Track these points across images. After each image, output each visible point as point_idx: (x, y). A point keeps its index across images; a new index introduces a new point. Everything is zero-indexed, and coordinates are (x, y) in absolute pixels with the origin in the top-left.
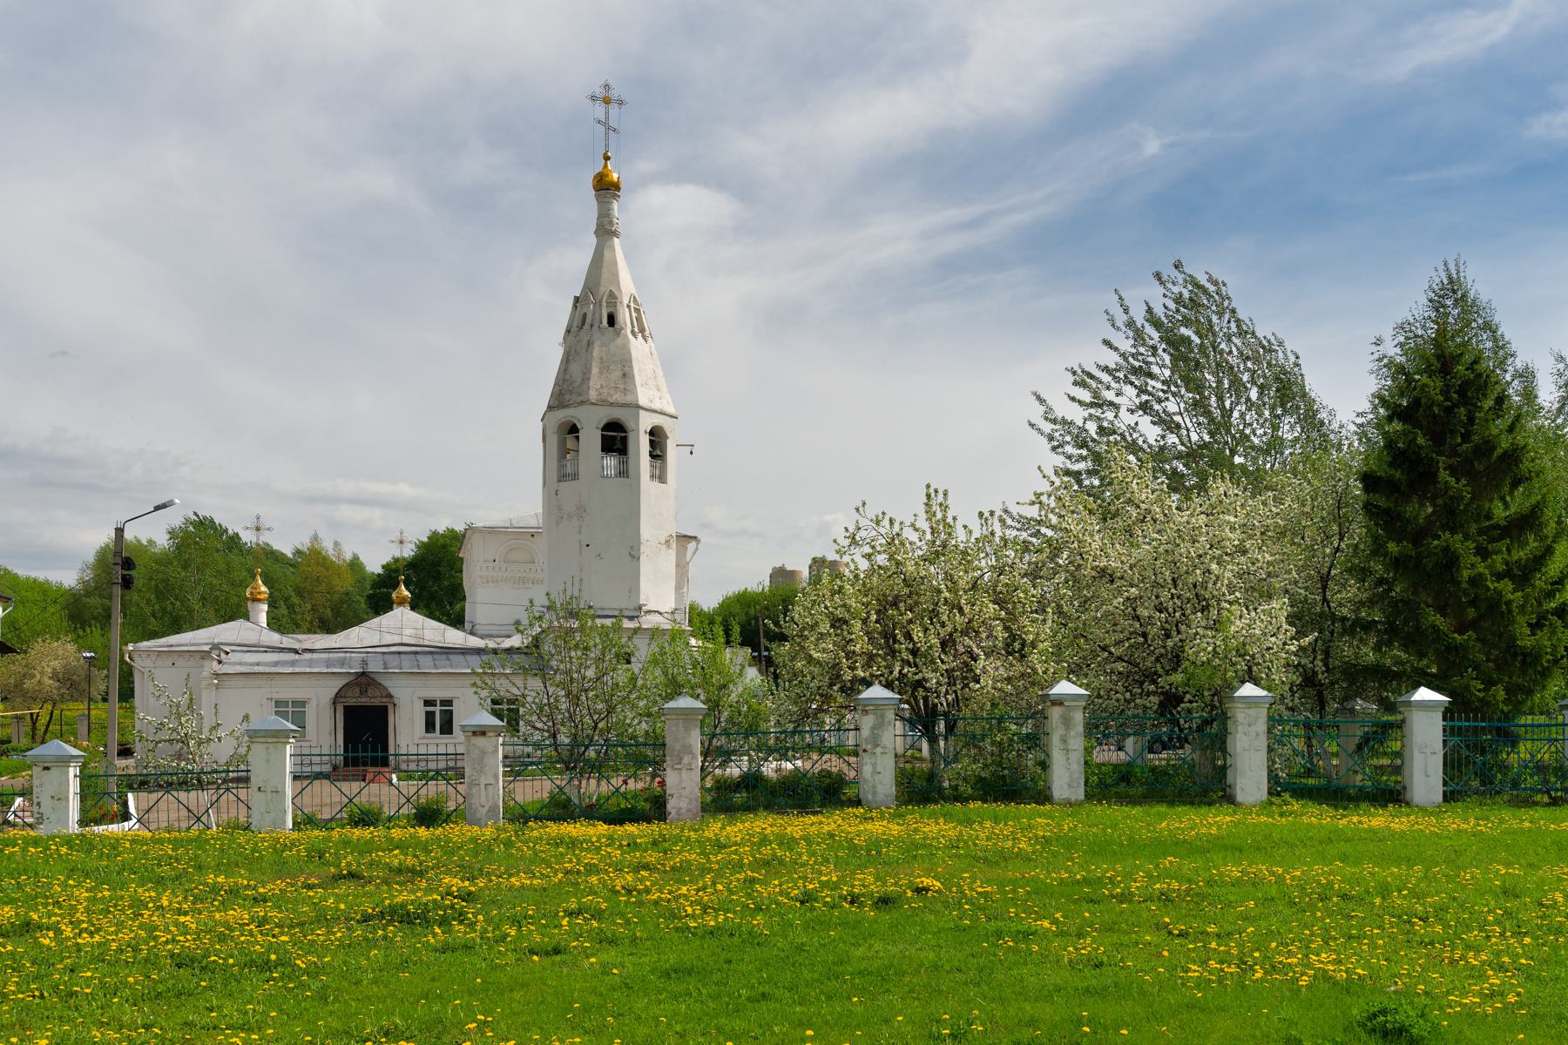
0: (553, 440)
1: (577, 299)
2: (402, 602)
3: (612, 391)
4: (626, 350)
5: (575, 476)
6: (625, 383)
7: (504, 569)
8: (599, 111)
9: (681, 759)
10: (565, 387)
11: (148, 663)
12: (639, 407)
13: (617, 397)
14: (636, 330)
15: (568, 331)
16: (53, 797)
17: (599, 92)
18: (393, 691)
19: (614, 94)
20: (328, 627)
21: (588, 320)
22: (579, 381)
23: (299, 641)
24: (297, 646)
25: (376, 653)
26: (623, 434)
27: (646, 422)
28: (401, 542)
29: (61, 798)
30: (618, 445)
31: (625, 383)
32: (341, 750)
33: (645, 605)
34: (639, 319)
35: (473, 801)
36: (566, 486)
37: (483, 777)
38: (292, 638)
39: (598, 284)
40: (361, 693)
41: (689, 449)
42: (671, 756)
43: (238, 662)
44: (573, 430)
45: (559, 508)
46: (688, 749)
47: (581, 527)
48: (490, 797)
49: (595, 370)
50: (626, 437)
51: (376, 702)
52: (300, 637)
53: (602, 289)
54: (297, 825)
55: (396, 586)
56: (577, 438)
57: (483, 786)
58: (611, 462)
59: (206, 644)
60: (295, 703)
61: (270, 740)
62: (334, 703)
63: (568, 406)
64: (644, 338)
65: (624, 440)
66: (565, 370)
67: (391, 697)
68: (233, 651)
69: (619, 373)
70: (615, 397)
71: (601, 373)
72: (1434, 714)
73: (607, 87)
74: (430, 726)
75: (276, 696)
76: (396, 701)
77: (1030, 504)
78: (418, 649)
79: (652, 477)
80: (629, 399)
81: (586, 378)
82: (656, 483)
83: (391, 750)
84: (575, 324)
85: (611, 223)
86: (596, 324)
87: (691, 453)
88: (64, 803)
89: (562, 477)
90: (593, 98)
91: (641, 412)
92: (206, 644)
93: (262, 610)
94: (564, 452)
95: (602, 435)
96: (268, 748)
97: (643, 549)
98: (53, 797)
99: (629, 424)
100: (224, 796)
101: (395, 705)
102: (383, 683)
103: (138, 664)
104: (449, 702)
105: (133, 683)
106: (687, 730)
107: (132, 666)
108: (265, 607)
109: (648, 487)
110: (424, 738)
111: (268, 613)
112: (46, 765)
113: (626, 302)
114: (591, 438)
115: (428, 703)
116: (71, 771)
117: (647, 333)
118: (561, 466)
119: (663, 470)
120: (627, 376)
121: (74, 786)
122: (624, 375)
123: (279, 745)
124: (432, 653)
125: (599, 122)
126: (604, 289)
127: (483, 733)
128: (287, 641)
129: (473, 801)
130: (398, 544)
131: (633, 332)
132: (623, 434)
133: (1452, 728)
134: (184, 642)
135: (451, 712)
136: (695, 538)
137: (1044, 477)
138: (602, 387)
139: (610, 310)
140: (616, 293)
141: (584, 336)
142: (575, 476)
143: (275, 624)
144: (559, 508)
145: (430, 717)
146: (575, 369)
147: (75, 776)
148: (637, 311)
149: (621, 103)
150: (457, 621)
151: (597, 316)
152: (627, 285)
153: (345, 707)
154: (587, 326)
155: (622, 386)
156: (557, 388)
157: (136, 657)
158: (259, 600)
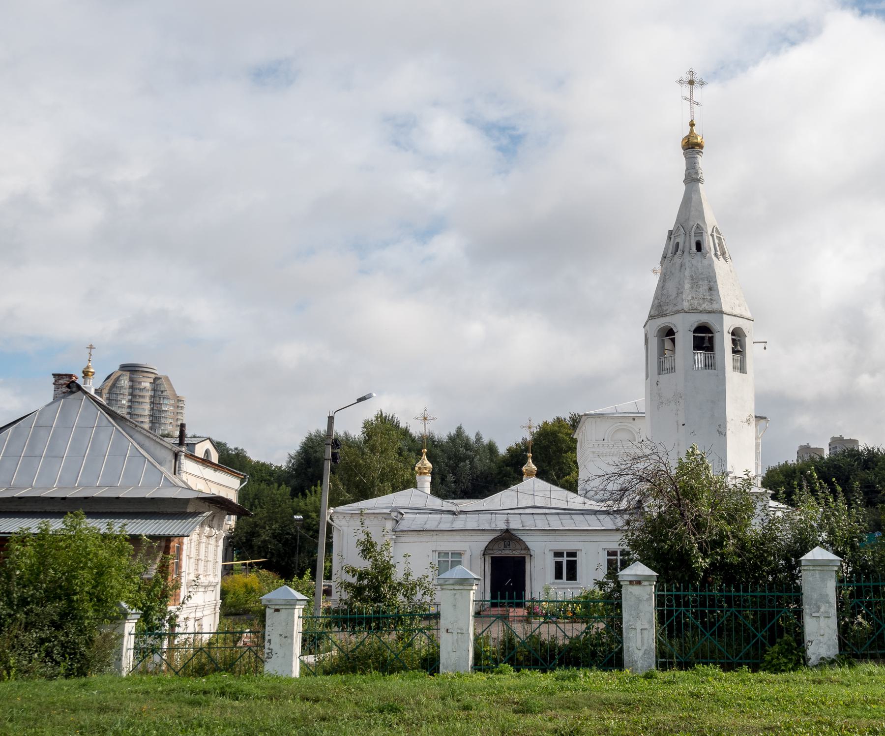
0: (654, 342)
1: (671, 233)
2: (530, 474)
3: (701, 301)
4: (711, 266)
5: (672, 369)
6: (711, 295)
7: (611, 446)
8: (686, 90)
9: (819, 607)
10: (663, 300)
11: (343, 522)
12: (722, 313)
13: (706, 306)
14: (719, 253)
15: (664, 257)
16: (281, 635)
17: (686, 77)
18: (529, 544)
19: (696, 78)
20: (467, 494)
21: (680, 247)
22: (674, 294)
23: (456, 505)
24: (454, 509)
25: (514, 514)
27: (729, 323)
28: (425, 419)
29: (287, 637)
30: (706, 344)
31: (711, 295)
32: (488, 596)
33: (731, 472)
34: (720, 244)
35: (631, 644)
36: (665, 377)
37: (639, 622)
38: (447, 502)
39: (687, 220)
40: (505, 547)
41: (763, 345)
42: (809, 604)
43: (410, 521)
44: (669, 333)
45: (660, 396)
46: (824, 598)
47: (678, 410)
48: (645, 642)
49: (687, 286)
50: (712, 337)
51: (516, 553)
52: (456, 501)
53: (691, 223)
54: (481, 662)
55: (524, 462)
56: (673, 340)
57: (639, 631)
58: (700, 357)
59: (387, 508)
60: (454, 554)
61: (457, 587)
62: (484, 554)
63: (666, 315)
64: (725, 259)
65: (711, 340)
66: (663, 287)
67: (529, 549)
68: (406, 513)
69: (706, 287)
70: (703, 306)
71: (692, 287)
73: (691, 72)
74: (558, 575)
75: (439, 549)
76: (532, 553)
78: (547, 511)
79: (735, 368)
80: (715, 307)
81: (679, 293)
82: (737, 374)
83: (528, 596)
84: (670, 251)
85: (697, 173)
86: (687, 250)
87: (765, 348)
88: (289, 641)
89: (661, 371)
90: (681, 82)
91: (724, 315)
92: (387, 508)
93: (426, 481)
94: (662, 353)
95: (694, 336)
96: (455, 594)
97: (728, 426)
98: (281, 635)
99: (715, 326)
101: (531, 556)
102: (521, 538)
103: (336, 524)
104: (572, 554)
105: (332, 537)
106: (823, 580)
107: (332, 525)
108: (429, 478)
109: (732, 377)
110: (553, 584)
111: (432, 483)
112: (277, 607)
113: (710, 232)
114: (685, 339)
115: (558, 554)
116: (296, 611)
117: (727, 256)
118: (660, 363)
119: (743, 362)
120: (712, 288)
121: (298, 626)
122: (710, 289)
123: (464, 592)
124: (558, 514)
125: (686, 99)
126: (693, 223)
127: (639, 583)
128: (448, 505)
129: (631, 644)
130: (422, 421)
131: (716, 255)
134: (370, 506)
135: (575, 561)
136: (765, 418)
137: (91, 355)
138: (693, 298)
139: (698, 238)
140: (702, 225)
141: (677, 260)
142: (672, 369)
143: (437, 491)
144: (660, 396)
145: (558, 566)
146: (671, 286)
147: (299, 617)
148: (719, 239)
150: (572, 487)
151: (687, 244)
152: (711, 219)
153: (492, 558)
154: (679, 253)
155: (709, 297)
156: (656, 302)
157: (335, 518)
158: (425, 473)
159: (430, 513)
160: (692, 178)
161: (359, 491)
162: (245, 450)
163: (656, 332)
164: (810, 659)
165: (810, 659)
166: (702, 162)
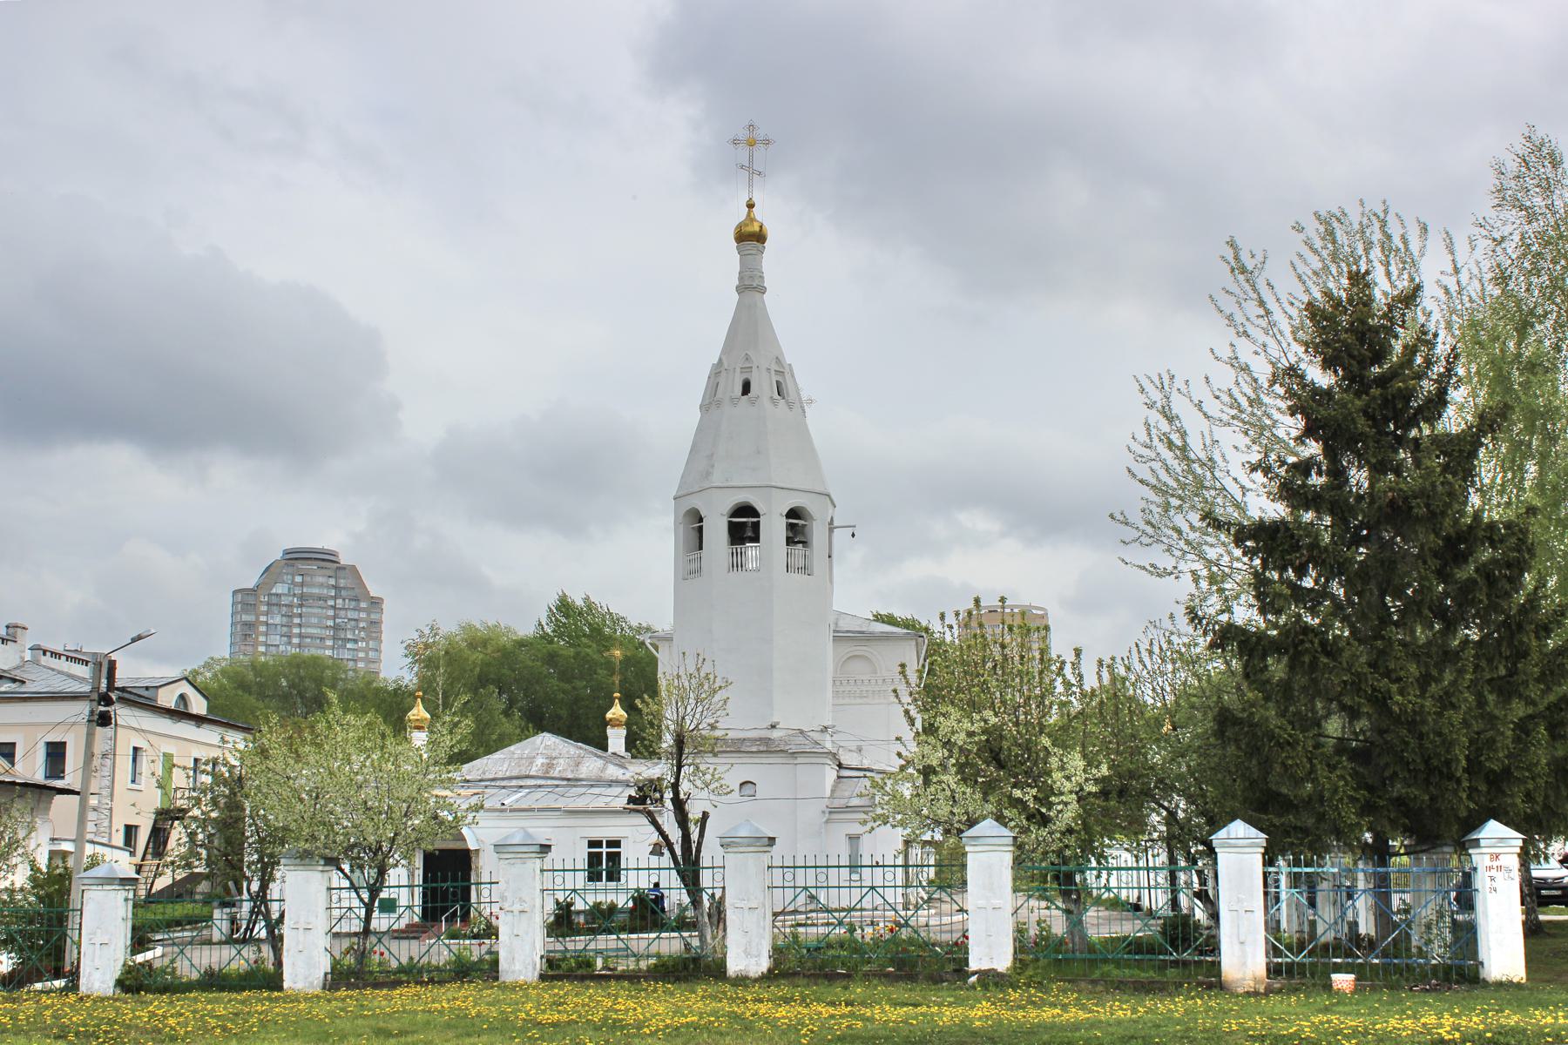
8: (743, 154)
17: (743, 134)
19: (761, 133)
26: (755, 520)
41: (850, 531)
65: (756, 526)
72: (299, 986)
77: (1142, 445)
87: (853, 535)
95: (730, 522)
100: (436, 947)
104: (615, 843)
114: (716, 531)
115: (592, 844)
132: (755, 520)
133: (434, 890)
139: (745, 376)
145: (594, 860)
149: (767, 142)
159: (557, 786)
160: (750, 285)
161: (1422, 739)
162: (1492, 181)
163: (681, 518)
164: (63, 778)
165: (63, 778)
166: (771, 258)
